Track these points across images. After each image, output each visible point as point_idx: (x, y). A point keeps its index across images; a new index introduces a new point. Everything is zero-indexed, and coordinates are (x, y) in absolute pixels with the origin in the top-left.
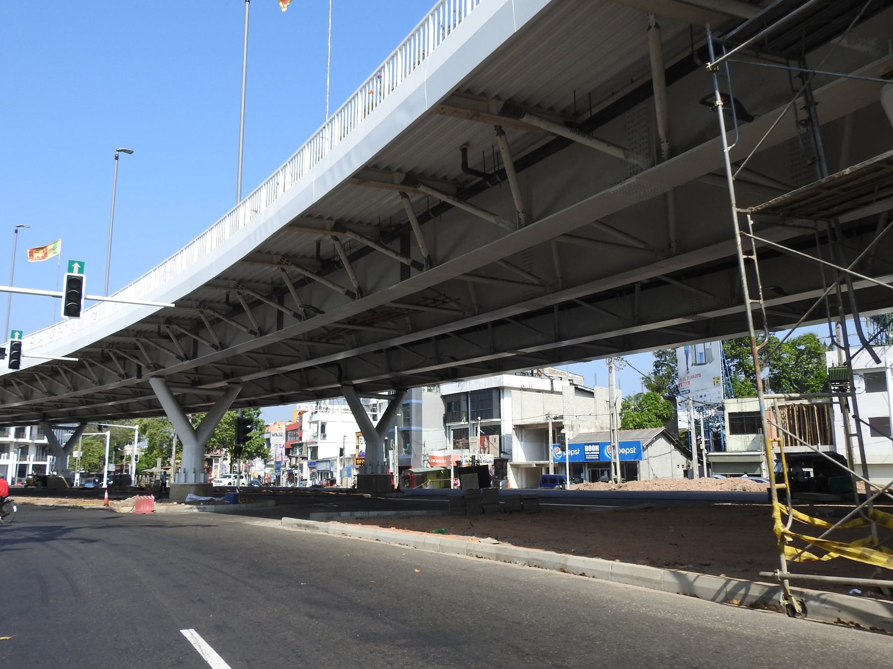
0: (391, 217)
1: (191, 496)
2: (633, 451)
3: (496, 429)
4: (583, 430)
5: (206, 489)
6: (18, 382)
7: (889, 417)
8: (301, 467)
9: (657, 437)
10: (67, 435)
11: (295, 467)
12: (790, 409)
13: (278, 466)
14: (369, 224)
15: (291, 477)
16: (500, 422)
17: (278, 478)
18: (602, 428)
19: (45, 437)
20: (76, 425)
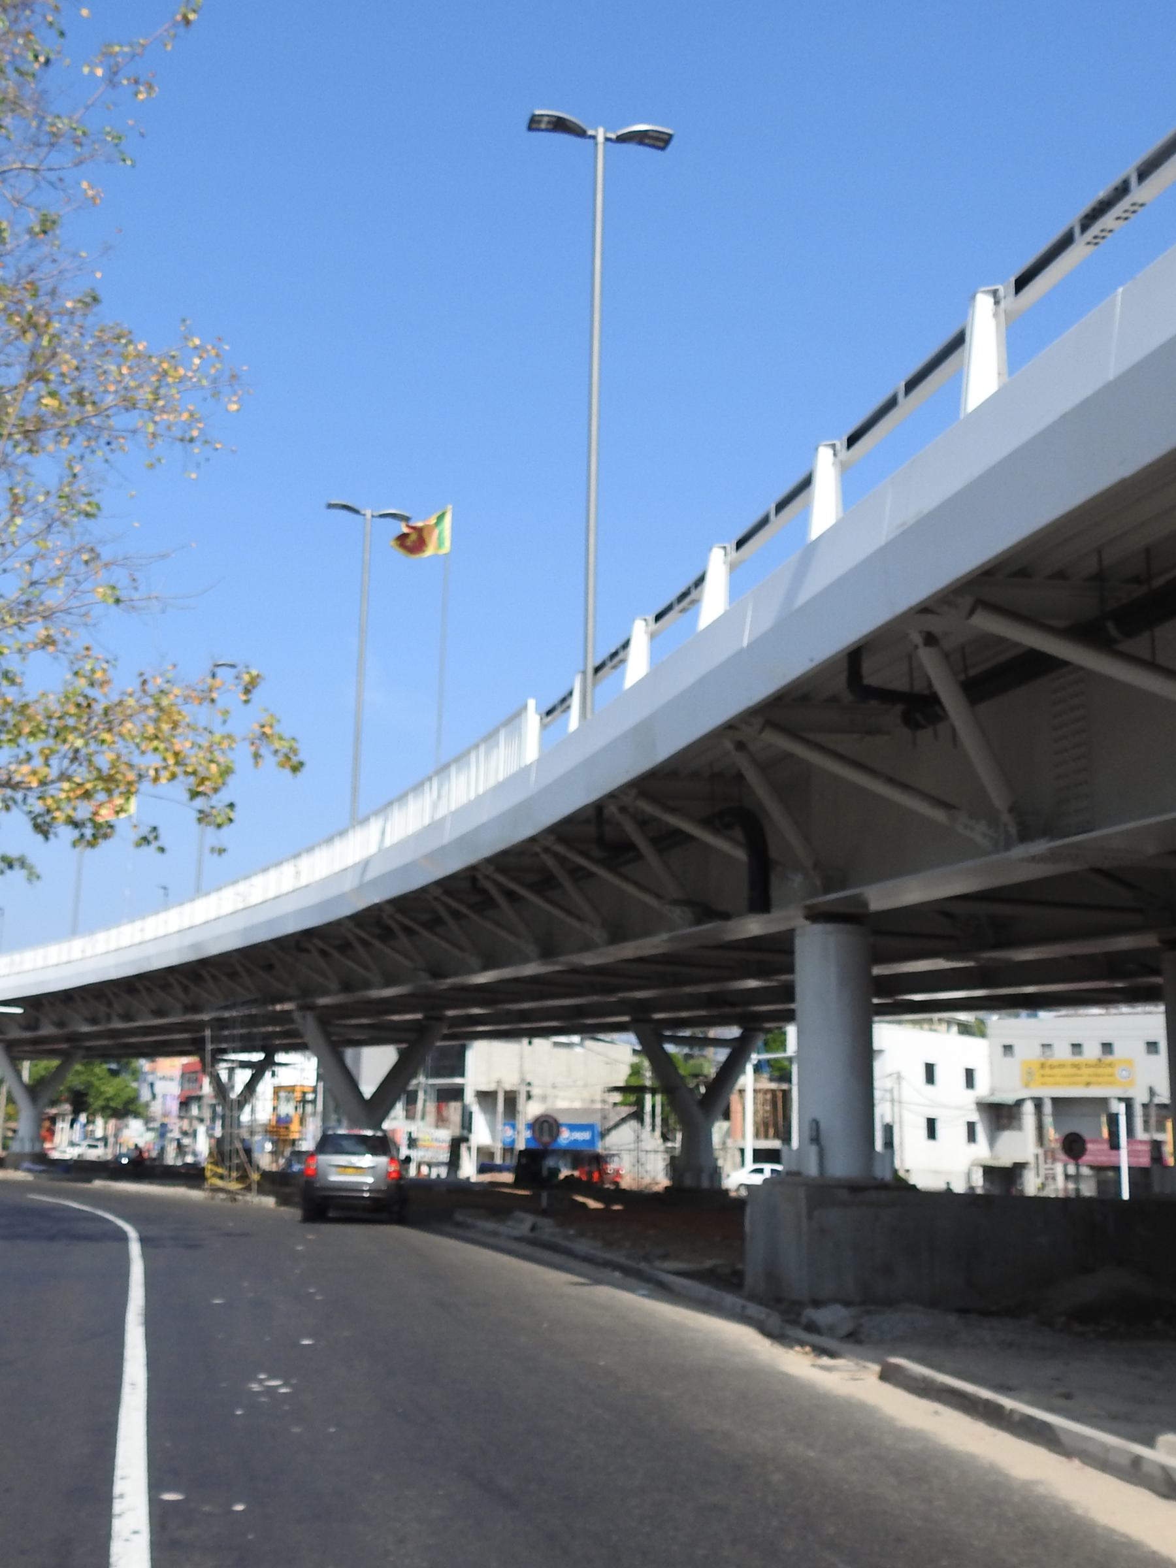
0: (1148, 551)
1: (26, 1165)
2: (585, 1136)
3: (457, 1093)
4: (562, 1104)
5: (41, 1158)
6: (580, 868)
7: (438, 1090)
8: (194, 1134)
9: (623, 1120)
10: (243, 1077)
11: (185, 1133)
12: (773, 1092)
13: (163, 1131)
14: (1061, 575)
15: (181, 1148)
16: (1038, 1103)
17: (162, 1150)
18: (593, 1101)
19: (1169, 1125)
20: (257, 1057)
